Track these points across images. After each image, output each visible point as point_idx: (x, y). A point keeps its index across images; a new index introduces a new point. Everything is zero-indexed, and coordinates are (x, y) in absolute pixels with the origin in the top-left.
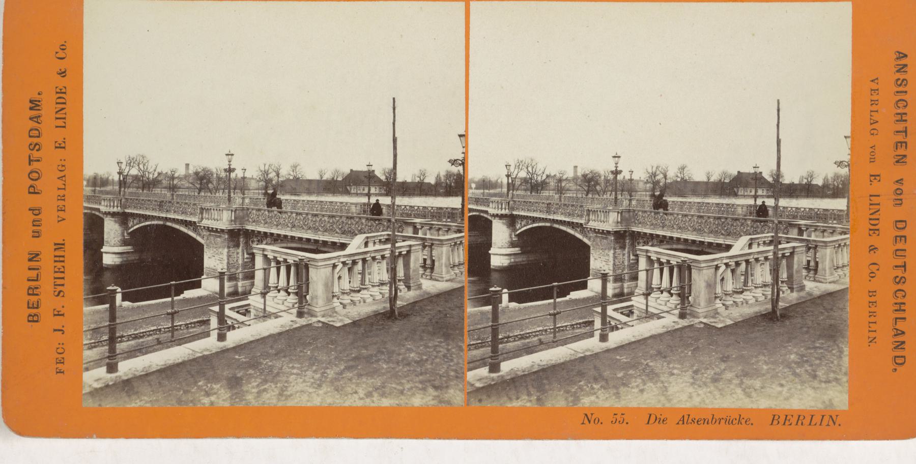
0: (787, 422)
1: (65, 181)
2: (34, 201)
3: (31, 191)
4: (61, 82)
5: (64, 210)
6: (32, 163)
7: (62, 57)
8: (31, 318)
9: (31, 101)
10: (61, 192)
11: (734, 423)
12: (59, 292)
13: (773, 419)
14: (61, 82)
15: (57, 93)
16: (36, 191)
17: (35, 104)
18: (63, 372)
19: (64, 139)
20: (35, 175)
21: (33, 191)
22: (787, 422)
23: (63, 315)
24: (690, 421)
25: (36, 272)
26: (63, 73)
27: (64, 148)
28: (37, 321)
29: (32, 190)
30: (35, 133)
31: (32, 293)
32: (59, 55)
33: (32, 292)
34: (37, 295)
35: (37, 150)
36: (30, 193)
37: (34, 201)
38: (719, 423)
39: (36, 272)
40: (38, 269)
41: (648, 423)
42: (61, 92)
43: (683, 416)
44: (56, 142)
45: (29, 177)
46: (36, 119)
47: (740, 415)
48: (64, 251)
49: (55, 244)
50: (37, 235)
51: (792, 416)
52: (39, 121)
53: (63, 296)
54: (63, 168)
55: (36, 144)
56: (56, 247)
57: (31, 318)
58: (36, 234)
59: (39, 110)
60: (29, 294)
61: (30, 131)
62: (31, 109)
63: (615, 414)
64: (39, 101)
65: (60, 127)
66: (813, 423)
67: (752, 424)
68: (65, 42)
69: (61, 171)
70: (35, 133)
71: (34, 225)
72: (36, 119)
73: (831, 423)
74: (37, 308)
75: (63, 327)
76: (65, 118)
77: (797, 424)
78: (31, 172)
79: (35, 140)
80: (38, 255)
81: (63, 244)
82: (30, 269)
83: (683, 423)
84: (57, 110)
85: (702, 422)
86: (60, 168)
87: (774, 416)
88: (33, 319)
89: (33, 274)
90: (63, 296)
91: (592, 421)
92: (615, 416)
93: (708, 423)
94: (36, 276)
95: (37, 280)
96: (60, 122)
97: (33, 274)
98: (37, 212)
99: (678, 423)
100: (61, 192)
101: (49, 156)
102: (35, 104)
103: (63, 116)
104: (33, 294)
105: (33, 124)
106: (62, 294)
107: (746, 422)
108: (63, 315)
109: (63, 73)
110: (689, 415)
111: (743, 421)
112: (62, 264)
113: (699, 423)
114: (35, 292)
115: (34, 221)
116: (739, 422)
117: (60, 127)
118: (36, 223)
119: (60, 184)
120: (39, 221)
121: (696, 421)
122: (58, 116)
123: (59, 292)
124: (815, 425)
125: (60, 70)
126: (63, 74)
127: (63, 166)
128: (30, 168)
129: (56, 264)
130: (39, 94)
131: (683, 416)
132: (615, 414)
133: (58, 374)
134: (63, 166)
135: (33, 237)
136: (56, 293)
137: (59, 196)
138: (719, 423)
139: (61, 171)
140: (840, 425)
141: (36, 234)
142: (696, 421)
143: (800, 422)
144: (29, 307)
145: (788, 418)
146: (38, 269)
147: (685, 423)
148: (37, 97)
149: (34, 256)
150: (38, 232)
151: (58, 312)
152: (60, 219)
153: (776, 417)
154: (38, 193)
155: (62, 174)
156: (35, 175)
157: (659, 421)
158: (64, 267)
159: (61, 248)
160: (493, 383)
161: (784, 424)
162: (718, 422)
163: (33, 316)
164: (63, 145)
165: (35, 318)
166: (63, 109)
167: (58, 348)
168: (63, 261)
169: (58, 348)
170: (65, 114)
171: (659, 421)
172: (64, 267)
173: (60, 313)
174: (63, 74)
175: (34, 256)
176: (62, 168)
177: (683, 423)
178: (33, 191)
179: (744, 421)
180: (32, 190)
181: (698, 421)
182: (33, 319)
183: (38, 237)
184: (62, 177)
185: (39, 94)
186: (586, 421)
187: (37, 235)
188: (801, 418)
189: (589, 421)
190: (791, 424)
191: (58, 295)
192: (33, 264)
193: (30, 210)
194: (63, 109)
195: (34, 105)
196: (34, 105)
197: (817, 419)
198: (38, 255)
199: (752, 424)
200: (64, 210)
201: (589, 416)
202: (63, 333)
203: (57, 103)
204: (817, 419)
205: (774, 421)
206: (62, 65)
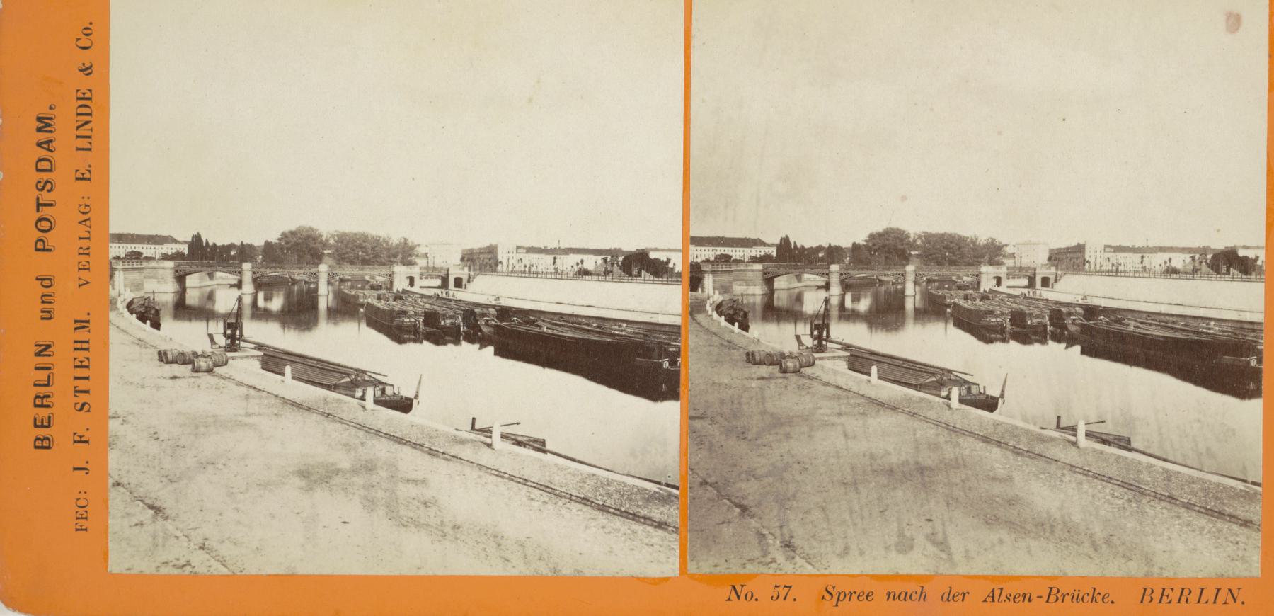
0: (1165, 598)
1: (90, 227)
2: (44, 264)
3: (38, 246)
4: (84, 83)
5: (88, 269)
6: (41, 208)
7: (87, 46)
8: (39, 444)
9: (39, 119)
10: (85, 243)
11: (913, 598)
12: (83, 405)
13: (1144, 594)
14: (84, 83)
15: (78, 99)
16: (47, 247)
17: (44, 124)
18: (86, 530)
19: (90, 166)
20: (45, 225)
21: (42, 247)
22: (1165, 600)
23: (87, 442)
24: (1003, 597)
25: (46, 373)
26: (87, 69)
27: (89, 179)
28: (48, 448)
29: (40, 245)
30: (44, 166)
31: (40, 403)
32: (81, 43)
33: (41, 401)
34: (48, 406)
35: (49, 191)
36: (37, 250)
37: (44, 264)
38: (850, 600)
39: (47, 372)
40: (49, 368)
41: (1199, 602)
42: (84, 98)
43: (993, 591)
44: (78, 91)
45: (36, 226)
46: (45, 144)
47: (1095, 589)
48: (89, 331)
49: (76, 321)
50: (47, 315)
51: (1172, 589)
52: (51, 148)
53: (89, 411)
54: (87, 209)
55: (47, 182)
56: (79, 325)
57: (39, 444)
58: (47, 315)
59: (51, 132)
60: (36, 406)
61: (37, 162)
62: (39, 130)
63: (776, 586)
64: (50, 119)
65: (83, 149)
66: (1203, 600)
67: (1112, 602)
68: (91, 24)
69: (83, 213)
70: (44, 166)
71: (43, 302)
72: (45, 144)
73: (1230, 599)
74: (48, 426)
75: (87, 462)
76: (90, 137)
77: (1179, 602)
78: (40, 220)
79: (45, 176)
80: (48, 346)
81: (88, 322)
82: (37, 368)
83: (993, 601)
84: (79, 123)
85: (1021, 598)
86: (82, 209)
87: (1145, 589)
88: (43, 444)
89: (42, 376)
90: (89, 411)
91: (742, 597)
92: (777, 589)
93: (1029, 601)
94: (46, 379)
95: (48, 385)
96: (83, 143)
97: (42, 376)
98: (47, 283)
99: (985, 601)
100: (85, 243)
101: (66, 193)
102: (44, 124)
103: (88, 133)
104: (42, 406)
105: (43, 153)
106: (86, 408)
107: (1103, 598)
108: (87, 442)
109: (87, 69)
110: (1002, 589)
111: (1099, 598)
112: (85, 354)
113: (1017, 600)
114: (45, 403)
115: (43, 296)
116: (1093, 599)
117: (83, 149)
118: (46, 299)
119: (82, 230)
120: (51, 295)
121: (1011, 598)
122: (80, 133)
123: (83, 405)
124: (1207, 602)
125: (84, 64)
126: (87, 70)
127: (86, 206)
128: (38, 215)
129: (78, 354)
130: (51, 108)
131: (993, 591)
132: (776, 586)
133: (81, 271)
134: (86, 206)
135: (42, 319)
136: (78, 407)
137: (81, 248)
138: (850, 600)
139: (83, 213)
140: (1243, 603)
141: (47, 315)
142: (1011, 598)
143: (1183, 599)
144: (36, 426)
145: (1165, 593)
146: (49, 368)
147: (996, 599)
148: (47, 113)
149: (44, 350)
150: (49, 312)
151: (81, 437)
152: (82, 282)
153: (1149, 592)
154: (49, 250)
155: (86, 217)
156: (45, 225)
157: (1077, 599)
158: (88, 359)
159: (84, 327)
160: (1242, 499)
161: (1160, 602)
162: (848, 597)
163: (42, 441)
164: (87, 175)
165: (46, 444)
166: (87, 123)
167: (78, 499)
168: (87, 349)
169: (78, 499)
170: (91, 130)
171: (1077, 599)
172: (88, 359)
173: (83, 439)
174: (87, 70)
175: (44, 350)
176: (85, 209)
177: (993, 601)
178: (42, 247)
179: (1101, 596)
180: (40, 245)
181: (1015, 598)
182: (43, 444)
183: (50, 318)
184: (85, 221)
185: (51, 108)
186: (734, 596)
187: (47, 315)
188: (1186, 592)
189: (738, 597)
190: (1170, 602)
191: (81, 409)
192: (42, 361)
193: (37, 279)
194: (87, 123)
195: (43, 125)
196: (43, 125)
197: (1209, 595)
198: (48, 346)
199: (1112, 602)
200: (88, 269)
201: (739, 588)
202: (87, 473)
203: (79, 114)
204: (1209, 595)
205: (1051, 596)
206: (86, 58)
